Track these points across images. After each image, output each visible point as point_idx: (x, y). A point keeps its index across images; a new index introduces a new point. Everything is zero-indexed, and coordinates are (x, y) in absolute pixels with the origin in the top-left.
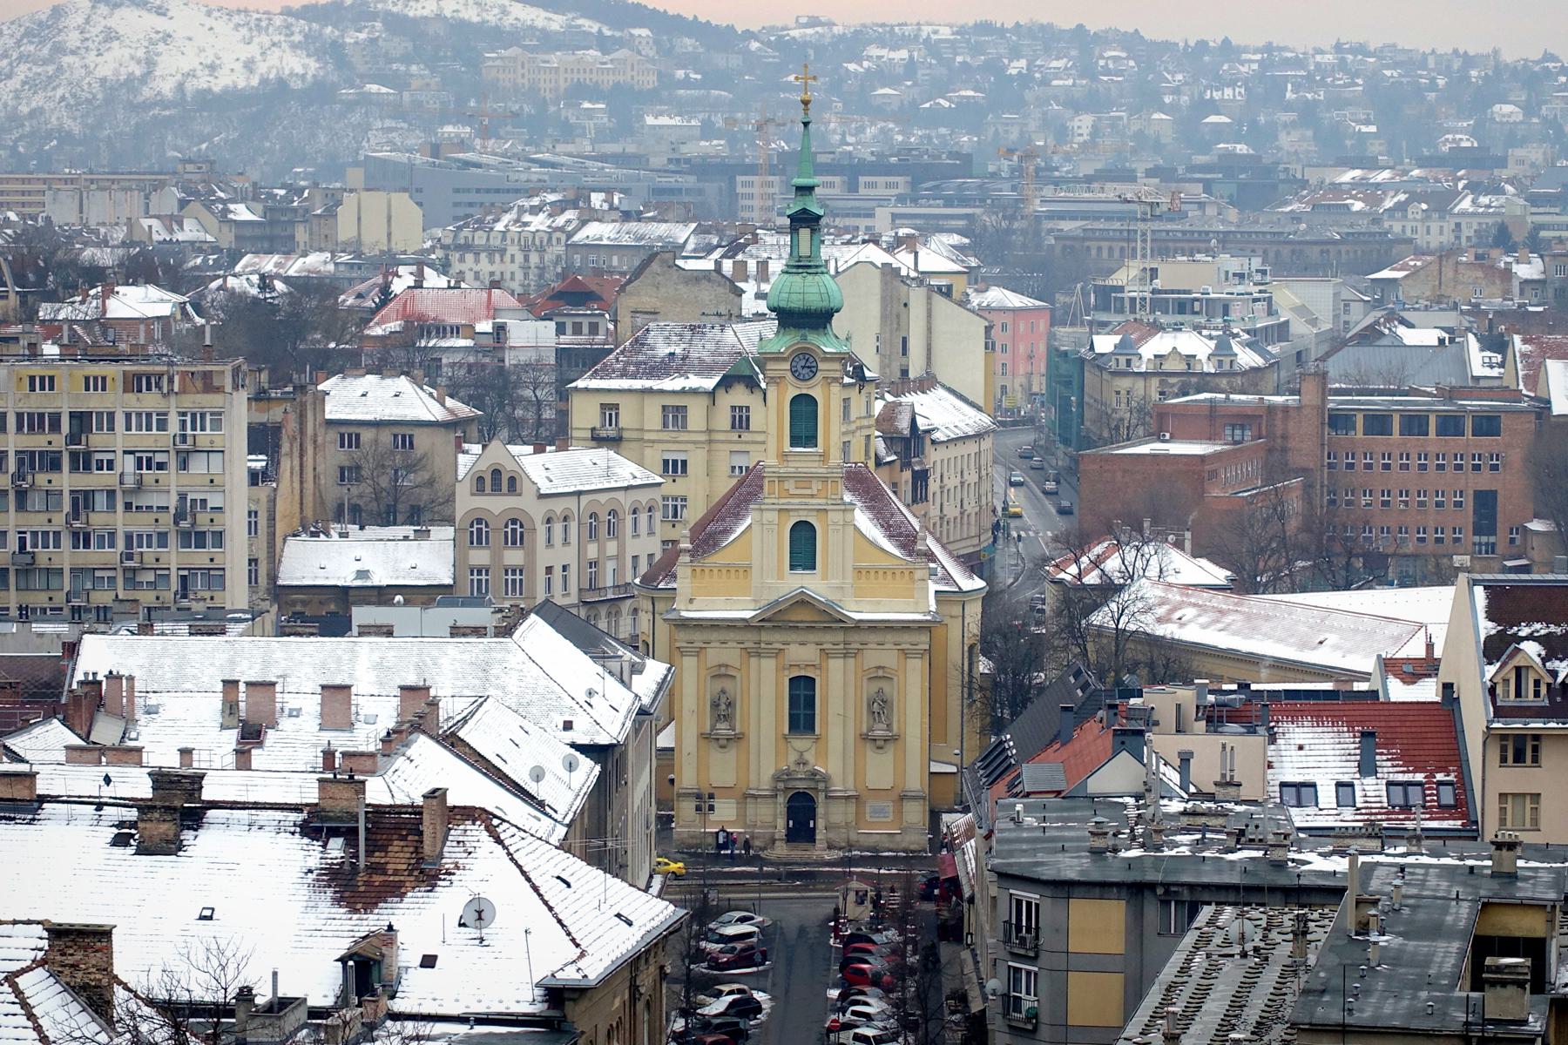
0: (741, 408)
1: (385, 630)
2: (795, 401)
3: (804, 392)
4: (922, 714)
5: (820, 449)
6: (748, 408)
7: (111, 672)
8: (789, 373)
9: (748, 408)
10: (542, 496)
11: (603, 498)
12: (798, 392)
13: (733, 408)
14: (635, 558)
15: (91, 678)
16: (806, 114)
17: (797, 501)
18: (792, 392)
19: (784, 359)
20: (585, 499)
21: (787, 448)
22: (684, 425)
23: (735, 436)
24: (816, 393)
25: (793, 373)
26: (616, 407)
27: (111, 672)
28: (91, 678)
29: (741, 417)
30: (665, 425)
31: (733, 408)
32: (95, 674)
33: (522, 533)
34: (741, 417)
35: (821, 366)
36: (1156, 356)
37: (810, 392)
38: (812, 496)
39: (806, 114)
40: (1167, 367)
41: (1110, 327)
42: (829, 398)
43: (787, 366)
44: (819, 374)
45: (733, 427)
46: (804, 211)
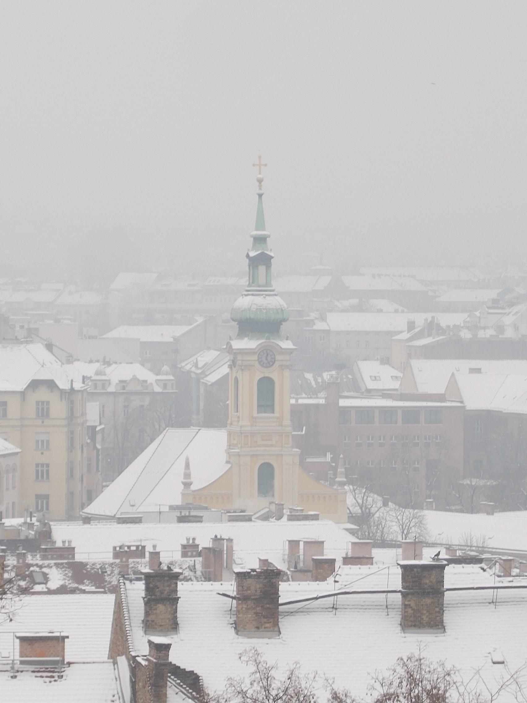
0: (43, 402)
3: (267, 375)
4: (505, 598)
5: (277, 414)
6: (48, 403)
7: (216, 536)
8: (257, 364)
9: (48, 403)
12: (262, 376)
13: (38, 403)
15: (191, 542)
16: (260, 189)
17: (263, 449)
18: (259, 376)
21: (255, 414)
23: (39, 422)
24: (275, 376)
25: (260, 363)
27: (216, 536)
28: (67, 545)
29: (43, 409)
31: (38, 403)
34: (43, 409)
35: (278, 357)
37: (271, 376)
38: (272, 446)
41: (506, 314)
43: (255, 358)
44: (276, 363)
46: (263, 254)
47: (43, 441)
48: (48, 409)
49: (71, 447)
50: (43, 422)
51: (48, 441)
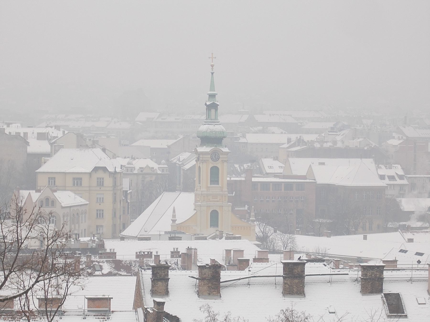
0: (100, 178)
1: (204, 238)
2: (212, 168)
3: (215, 165)
5: (220, 185)
6: (103, 178)
7: (188, 247)
9: (103, 178)
10: (63, 208)
11: (75, 208)
12: (213, 165)
13: (98, 178)
14: (82, 230)
15: (176, 250)
16: (212, 70)
18: (211, 166)
19: (209, 154)
20: (72, 209)
21: (209, 185)
22: (81, 184)
23: (98, 188)
24: (219, 166)
26: (54, 178)
27: (188, 247)
29: (100, 182)
30: (74, 185)
31: (98, 178)
32: (177, 249)
33: (55, 221)
34: (100, 182)
35: (221, 156)
36: (140, 168)
38: (218, 201)
39: (212, 70)
40: (145, 171)
42: (223, 169)
44: (220, 159)
45: (98, 185)
47: (100, 198)
48: (103, 182)
49: (115, 201)
50: (100, 188)
51: (103, 198)
